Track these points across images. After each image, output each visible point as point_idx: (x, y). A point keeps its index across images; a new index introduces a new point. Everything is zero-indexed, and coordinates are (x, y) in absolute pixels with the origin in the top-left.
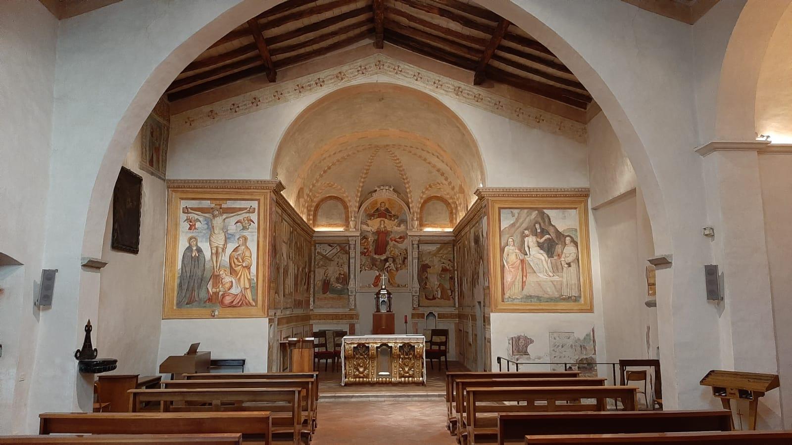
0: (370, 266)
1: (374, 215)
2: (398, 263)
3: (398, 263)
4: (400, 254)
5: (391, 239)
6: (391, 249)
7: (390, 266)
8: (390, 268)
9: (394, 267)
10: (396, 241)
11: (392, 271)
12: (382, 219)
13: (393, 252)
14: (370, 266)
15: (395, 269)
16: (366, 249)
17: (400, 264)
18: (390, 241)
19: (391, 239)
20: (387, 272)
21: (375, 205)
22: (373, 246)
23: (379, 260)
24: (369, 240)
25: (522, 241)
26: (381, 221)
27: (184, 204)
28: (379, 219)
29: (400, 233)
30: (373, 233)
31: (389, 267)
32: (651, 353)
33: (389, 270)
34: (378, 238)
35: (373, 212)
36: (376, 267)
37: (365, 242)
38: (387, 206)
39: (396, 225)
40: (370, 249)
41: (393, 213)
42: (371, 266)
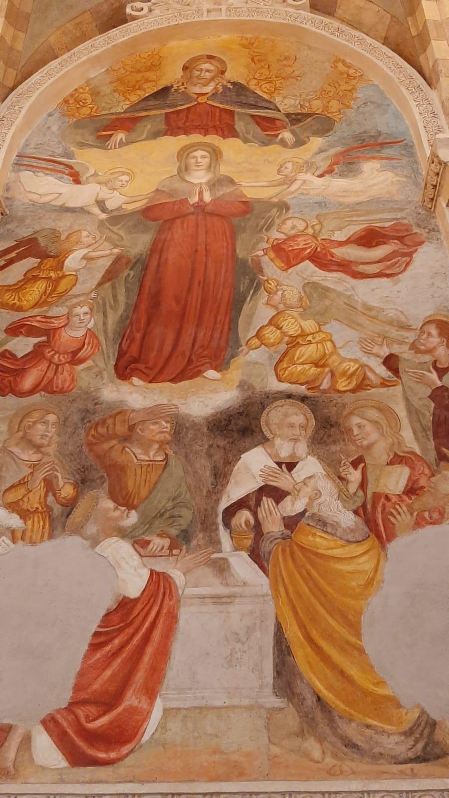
0: (49, 485)
1: (136, 120)
2: (380, 453)
3: (380, 453)
4: (391, 362)
5: (278, 249)
6: (291, 326)
7: (283, 481)
8: (292, 506)
9: (327, 487)
10: (322, 260)
11: (319, 541)
12: (196, 138)
13: (308, 351)
14: (49, 485)
15: (347, 519)
16: (31, 331)
17: (397, 459)
18: (271, 269)
19: (278, 249)
20: (256, 555)
21: (151, 75)
22: (100, 308)
23: (160, 429)
24: (72, 262)
25: (289, 601)
26: (184, 153)
27: (48, 350)
28: (173, 144)
29: (355, 208)
30: (117, 218)
31: (278, 495)
32: (254, 341)
33: (273, 526)
34: (157, 248)
35: (125, 105)
36: (125, 500)
37: (30, 278)
38: (236, 72)
39: (324, 166)
40: (73, 334)
41: (286, 103)
42: (67, 491)
